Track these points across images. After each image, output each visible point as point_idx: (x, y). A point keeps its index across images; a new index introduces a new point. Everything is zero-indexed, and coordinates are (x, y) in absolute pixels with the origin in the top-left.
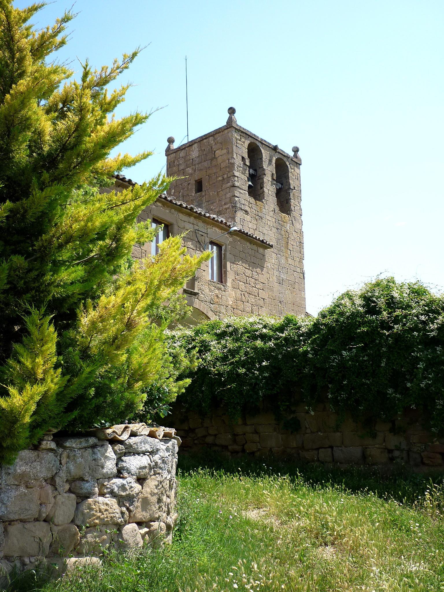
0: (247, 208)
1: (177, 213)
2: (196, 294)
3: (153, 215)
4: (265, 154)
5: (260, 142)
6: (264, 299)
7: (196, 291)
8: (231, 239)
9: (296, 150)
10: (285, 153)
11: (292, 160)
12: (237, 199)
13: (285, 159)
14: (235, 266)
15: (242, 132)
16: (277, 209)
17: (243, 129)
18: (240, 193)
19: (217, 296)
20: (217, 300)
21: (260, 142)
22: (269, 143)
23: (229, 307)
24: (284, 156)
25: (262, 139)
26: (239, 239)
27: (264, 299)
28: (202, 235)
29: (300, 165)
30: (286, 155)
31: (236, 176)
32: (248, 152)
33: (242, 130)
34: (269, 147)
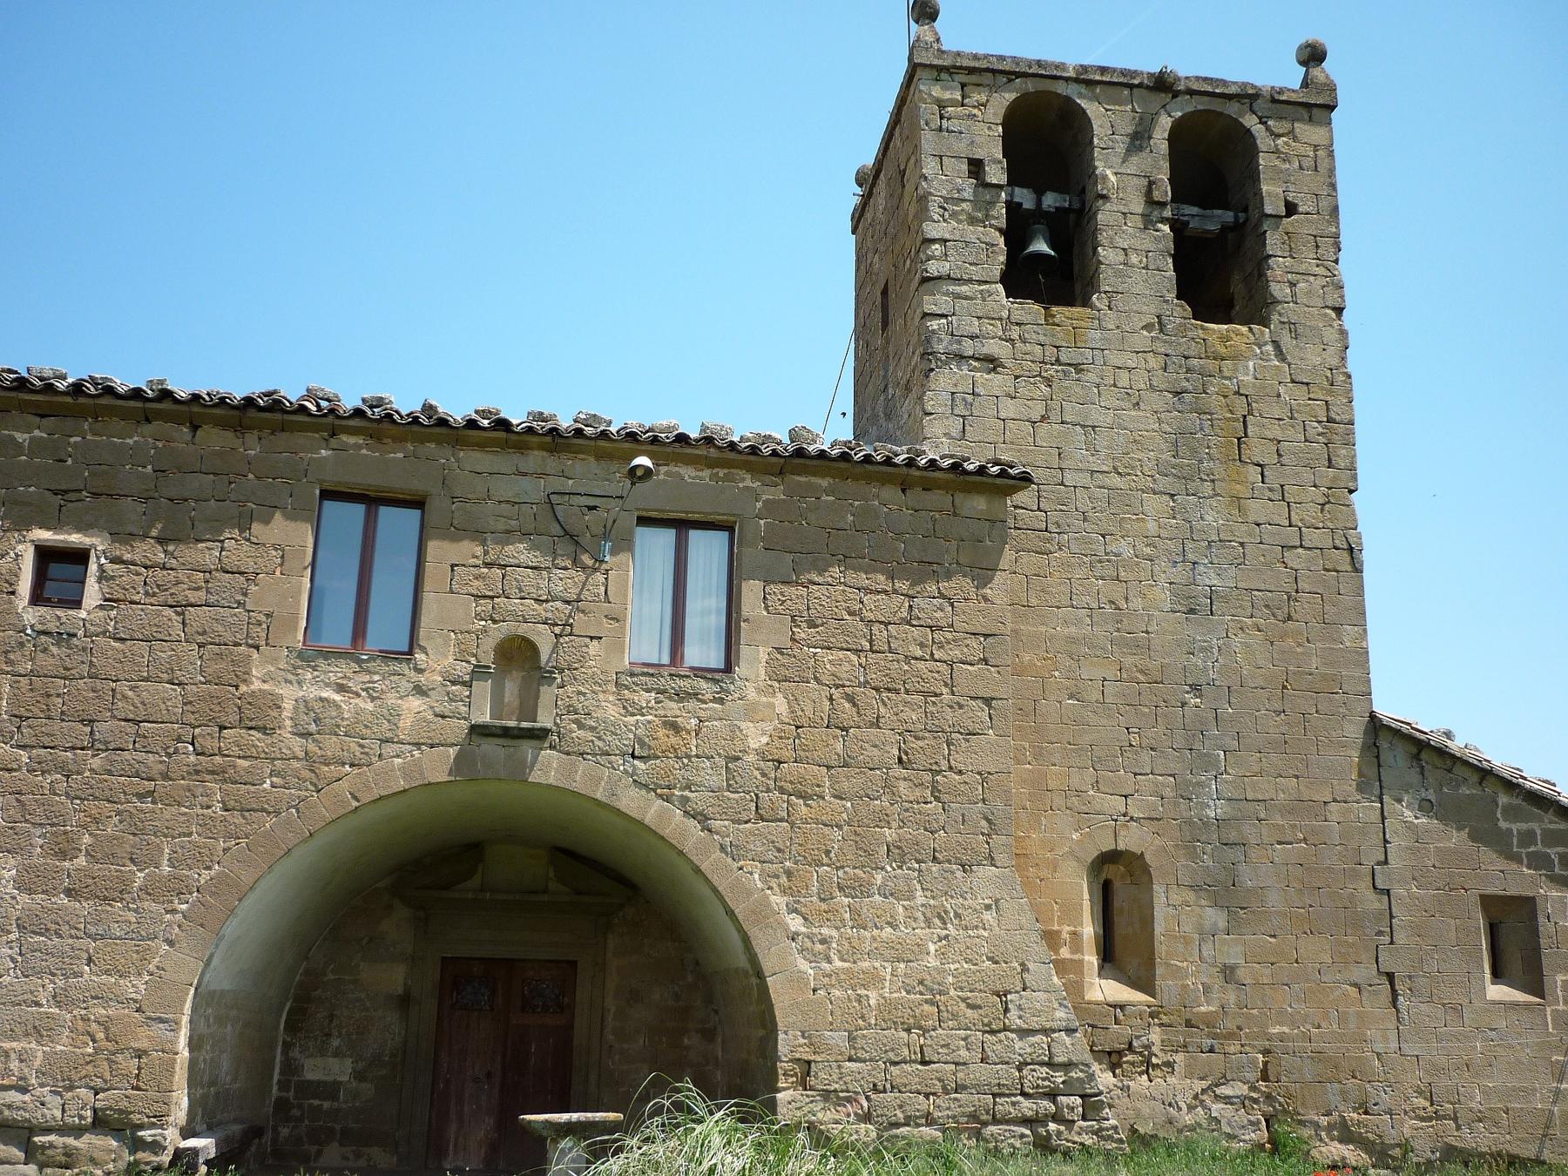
0: (993, 347)
1: (448, 451)
2: (540, 735)
3: (321, 482)
4: (1105, 122)
5: (1077, 80)
6: (988, 701)
7: (545, 720)
8: (777, 493)
9: (1313, 55)
10: (1224, 83)
11: (1274, 101)
12: (934, 324)
13: (1232, 109)
14: (791, 591)
15: (972, 71)
16: (1179, 312)
17: (976, 57)
18: (957, 296)
19: (675, 727)
20: (673, 740)
21: (1077, 80)
22: (1124, 73)
23: (751, 758)
24: (1229, 97)
25: (1085, 69)
26: (824, 483)
27: (988, 701)
28: (594, 508)
29: (1332, 108)
30: (1233, 90)
31: (933, 241)
32: (1006, 138)
33: (966, 63)
34: (1131, 87)
